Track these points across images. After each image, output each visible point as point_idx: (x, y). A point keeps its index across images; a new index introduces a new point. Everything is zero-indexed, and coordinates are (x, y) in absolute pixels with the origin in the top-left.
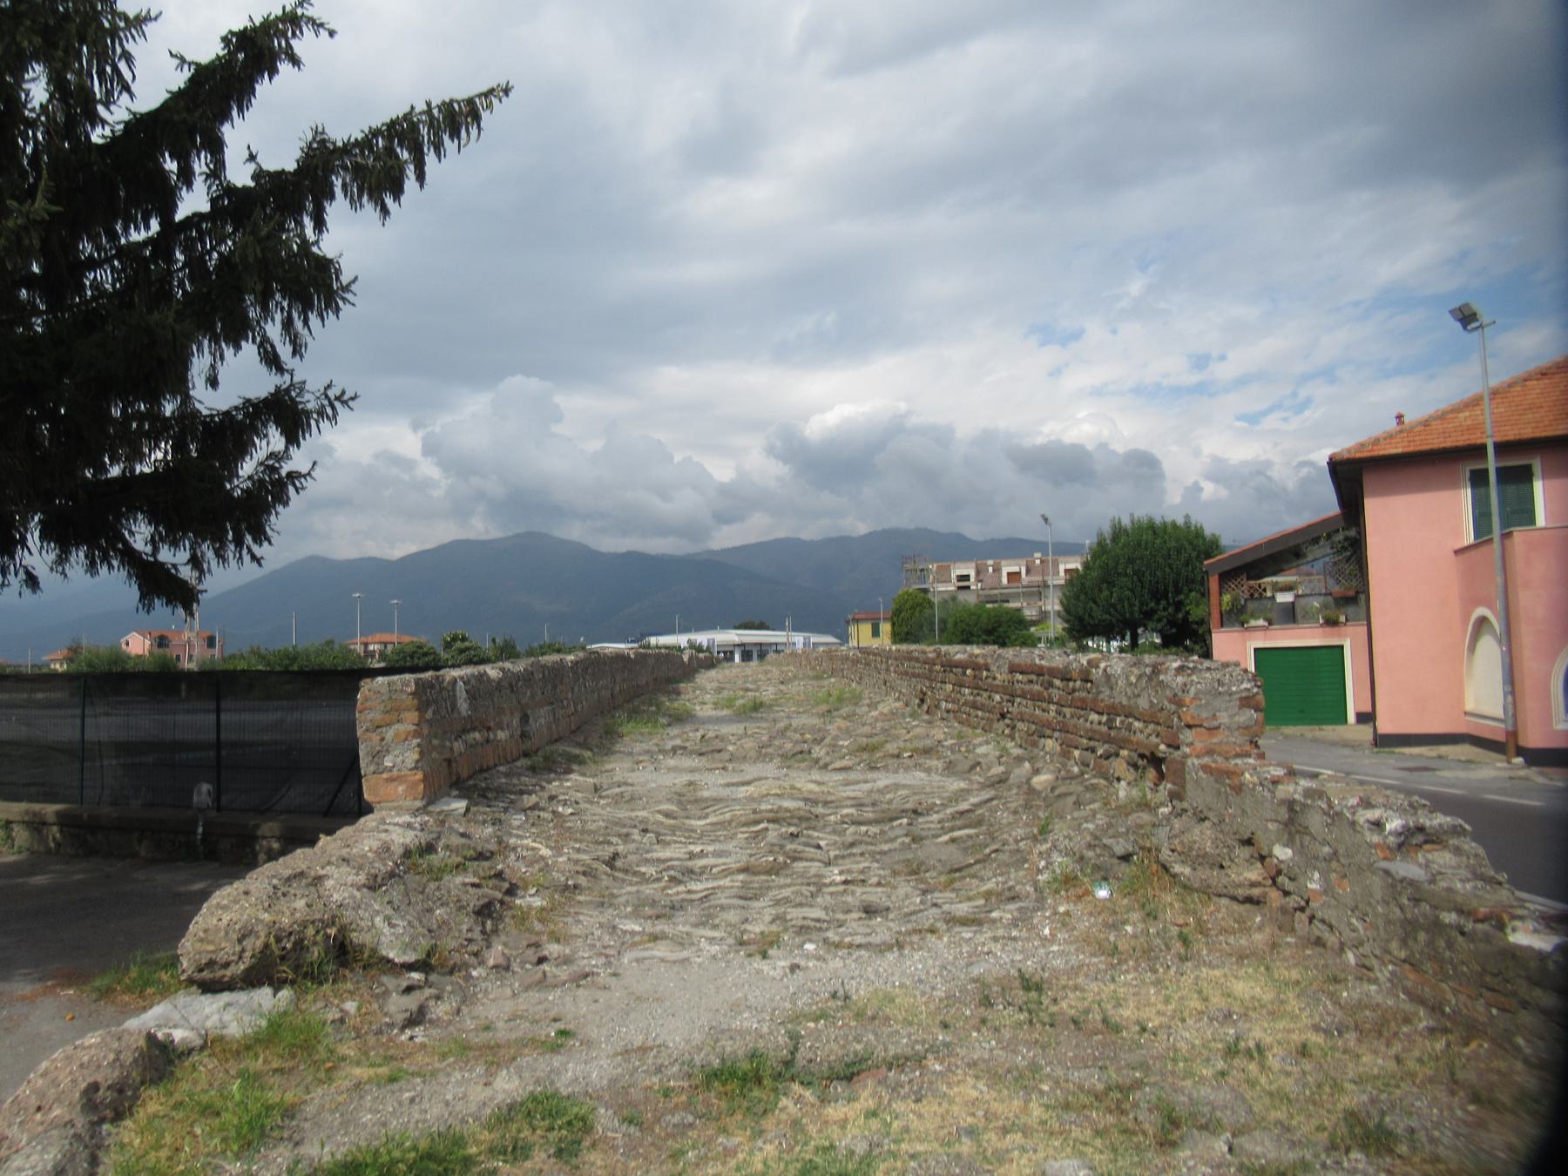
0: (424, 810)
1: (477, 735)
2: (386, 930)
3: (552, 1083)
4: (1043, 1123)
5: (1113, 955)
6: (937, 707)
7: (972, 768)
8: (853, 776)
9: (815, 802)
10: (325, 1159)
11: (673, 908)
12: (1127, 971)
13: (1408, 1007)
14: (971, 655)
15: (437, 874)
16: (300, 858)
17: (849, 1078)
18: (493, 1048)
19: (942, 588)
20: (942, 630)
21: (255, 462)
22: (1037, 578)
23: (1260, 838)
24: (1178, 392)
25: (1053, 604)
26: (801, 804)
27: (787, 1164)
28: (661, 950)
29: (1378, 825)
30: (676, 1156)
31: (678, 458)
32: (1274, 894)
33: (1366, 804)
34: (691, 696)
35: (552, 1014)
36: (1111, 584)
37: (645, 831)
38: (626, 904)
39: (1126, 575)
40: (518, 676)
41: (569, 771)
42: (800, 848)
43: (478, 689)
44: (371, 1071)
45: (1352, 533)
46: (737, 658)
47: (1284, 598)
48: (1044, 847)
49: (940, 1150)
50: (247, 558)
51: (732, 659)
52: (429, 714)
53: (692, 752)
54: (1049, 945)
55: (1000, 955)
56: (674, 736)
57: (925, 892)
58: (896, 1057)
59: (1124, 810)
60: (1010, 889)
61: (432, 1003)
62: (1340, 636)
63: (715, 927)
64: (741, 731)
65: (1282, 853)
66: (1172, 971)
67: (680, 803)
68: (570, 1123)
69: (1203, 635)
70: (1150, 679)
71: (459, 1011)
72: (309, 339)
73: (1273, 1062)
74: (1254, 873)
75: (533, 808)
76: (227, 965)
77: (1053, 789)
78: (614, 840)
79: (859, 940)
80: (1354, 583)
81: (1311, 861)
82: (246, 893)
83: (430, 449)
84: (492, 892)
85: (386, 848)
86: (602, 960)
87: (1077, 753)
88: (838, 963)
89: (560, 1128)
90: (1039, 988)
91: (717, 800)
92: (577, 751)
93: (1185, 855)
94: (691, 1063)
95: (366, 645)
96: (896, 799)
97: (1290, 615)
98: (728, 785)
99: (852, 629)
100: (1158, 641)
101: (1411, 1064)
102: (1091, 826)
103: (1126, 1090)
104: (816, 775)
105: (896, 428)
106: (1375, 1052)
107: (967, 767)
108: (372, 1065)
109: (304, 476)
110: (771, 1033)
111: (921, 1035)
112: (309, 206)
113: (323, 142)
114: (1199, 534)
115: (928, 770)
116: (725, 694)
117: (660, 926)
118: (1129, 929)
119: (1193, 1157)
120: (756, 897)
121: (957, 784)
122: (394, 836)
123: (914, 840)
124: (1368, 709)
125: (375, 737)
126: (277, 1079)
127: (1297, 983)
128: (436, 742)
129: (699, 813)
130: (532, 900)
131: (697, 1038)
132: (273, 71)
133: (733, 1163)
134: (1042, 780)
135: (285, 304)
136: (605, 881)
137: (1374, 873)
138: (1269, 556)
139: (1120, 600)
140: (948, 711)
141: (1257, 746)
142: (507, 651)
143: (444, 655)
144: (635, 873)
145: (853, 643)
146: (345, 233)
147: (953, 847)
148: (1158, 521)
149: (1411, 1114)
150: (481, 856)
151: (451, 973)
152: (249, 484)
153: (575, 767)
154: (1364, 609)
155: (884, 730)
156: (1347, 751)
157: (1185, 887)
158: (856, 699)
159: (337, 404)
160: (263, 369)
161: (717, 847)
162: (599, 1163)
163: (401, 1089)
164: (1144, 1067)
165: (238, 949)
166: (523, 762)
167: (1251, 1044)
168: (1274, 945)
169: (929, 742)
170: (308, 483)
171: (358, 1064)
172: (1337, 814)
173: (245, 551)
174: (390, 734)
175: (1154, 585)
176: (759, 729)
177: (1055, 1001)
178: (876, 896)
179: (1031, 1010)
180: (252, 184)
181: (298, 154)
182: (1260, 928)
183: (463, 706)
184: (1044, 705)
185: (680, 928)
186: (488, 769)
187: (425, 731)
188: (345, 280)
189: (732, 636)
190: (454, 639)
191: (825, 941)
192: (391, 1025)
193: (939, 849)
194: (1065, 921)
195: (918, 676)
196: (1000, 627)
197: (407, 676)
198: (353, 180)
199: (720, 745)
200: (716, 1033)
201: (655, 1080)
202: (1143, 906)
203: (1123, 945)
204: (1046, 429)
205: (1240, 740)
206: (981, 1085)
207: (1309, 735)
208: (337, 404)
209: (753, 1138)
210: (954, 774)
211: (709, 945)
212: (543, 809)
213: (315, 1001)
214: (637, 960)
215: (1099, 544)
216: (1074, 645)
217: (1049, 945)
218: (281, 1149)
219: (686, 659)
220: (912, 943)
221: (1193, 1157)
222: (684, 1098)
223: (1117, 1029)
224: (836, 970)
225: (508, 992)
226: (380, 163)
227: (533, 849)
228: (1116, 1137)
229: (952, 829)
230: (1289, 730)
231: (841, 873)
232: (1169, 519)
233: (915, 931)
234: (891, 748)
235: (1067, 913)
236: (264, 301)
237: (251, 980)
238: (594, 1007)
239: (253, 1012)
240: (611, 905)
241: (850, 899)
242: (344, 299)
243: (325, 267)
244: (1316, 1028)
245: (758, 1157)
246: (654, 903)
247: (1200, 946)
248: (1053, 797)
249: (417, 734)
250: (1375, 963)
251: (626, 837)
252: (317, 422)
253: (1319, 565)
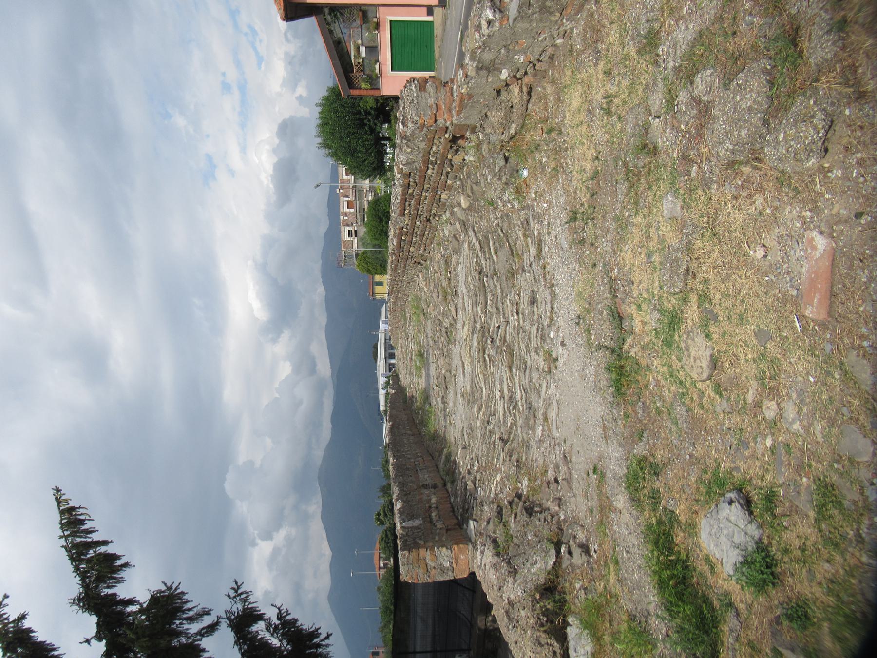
0: (474, 544)
1: (433, 514)
2: (538, 566)
3: (621, 478)
4: (644, 216)
5: (558, 172)
6: (422, 255)
7: (457, 239)
8: (460, 305)
9: (474, 328)
10: (656, 599)
11: (530, 408)
12: (567, 163)
13: (585, 14)
14: (394, 236)
15: (509, 537)
16: (498, 612)
17: (621, 318)
18: (602, 508)
19: (355, 246)
20: (380, 246)
21: (273, 639)
22: (351, 191)
23: (497, 85)
24: (244, 102)
25: (366, 184)
26: (475, 336)
27: (664, 354)
28: (552, 416)
29: (490, 22)
30: (659, 412)
31: (277, 395)
32: (526, 80)
33: (478, 28)
34: (414, 390)
35: (585, 476)
36: (355, 151)
37: (488, 422)
38: (527, 433)
39: (350, 142)
40: (401, 491)
41: (455, 461)
42: (499, 337)
43: (407, 514)
44: (612, 574)
45: (327, 10)
46: (393, 361)
47: (363, 52)
48: (500, 203)
49: (658, 273)
50: (327, 642)
51: (394, 365)
52: (421, 542)
53: (446, 393)
54: (553, 204)
55: (557, 232)
56: (437, 401)
57: (524, 271)
58: (611, 293)
59: (481, 158)
60: (522, 224)
61: (577, 540)
62: (385, 22)
63: (540, 385)
64: (434, 365)
65: (504, 74)
66: (567, 140)
67: (473, 402)
68: (641, 469)
69: (384, 100)
70: (409, 141)
71: (582, 526)
72: (200, 607)
73: (614, 90)
74: (515, 90)
75: (475, 484)
76: (554, 652)
77: (469, 197)
78: (493, 439)
79: (548, 308)
80: (355, 12)
81: (508, 60)
82: (516, 643)
83: (267, 536)
84: (519, 507)
85: (494, 566)
86: (557, 447)
87: (449, 182)
88: (561, 320)
89: (644, 473)
90: (575, 213)
91: (472, 382)
92: (444, 457)
93: (505, 127)
94: (612, 403)
95: (380, 568)
96: (473, 283)
97: (373, 49)
98: (464, 375)
99: (378, 297)
100: (387, 125)
101: (614, 16)
102: (489, 178)
103: (628, 171)
104: (459, 326)
105: (262, 268)
106: (608, 34)
107: (456, 242)
108: (609, 574)
109: (280, 611)
110: (597, 360)
111: (599, 279)
112: (120, 608)
113: (79, 599)
114: (327, 99)
115: (458, 264)
116: (413, 371)
117: (540, 415)
118: (544, 160)
119: (661, 137)
120: (525, 363)
121: (465, 249)
122: (488, 561)
123: (496, 275)
124: (425, 9)
125: (433, 572)
126: (615, 624)
127: (572, 71)
128: (437, 538)
129: (479, 392)
130: (524, 485)
131: (598, 399)
132: (30, 630)
133: (663, 382)
134: (464, 203)
135: (178, 622)
136: (515, 444)
137: (515, 27)
138: (340, 60)
139: (364, 146)
141: (447, 83)
142: (386, 490)
143: (388, 525)
144: (511, 428)
145: (386, 297)
146: (136, 587)
147: (499, 253)
148: (319, 122)
149: (639, 20)
150: (500, 513)
151: (562, 530)
152: (284, 641)
153: (452, 458)
154: (370, 8)
155: (435, 285)
156: (448, 23)
157: (522, 127)
158: (418, 299)
159: (239, 592)
160: (216, 633)
161: (497, 382)
162: (662, 453)
163: (622, 558)
164: (616, 159)
165: (546, 646)
166: (449, 486)
167: (604, 101)
168: (553, 82)
169: (442, 262)
170: (284, 609)
171: (608, 580)
172: (484, 44)
173: (323, 643)
174: (431, 564)
175: (356, 126)
176: (433, 354)
177: (582, 205)
178: (525, 297)
179: (587, 218)
180: (104, 641)
181: (86, 614)
182: (544, 89)
183: (417, 522)
184: (423, 198)
185: (541, 405)
186: (453, 508)
187: (431, 544)
188: (163, 588)
189: (381, 364)
190: (378, 519)
191: (549, 326)
192: (588, 562)
193: (501, 261)
194: (540, 195)
195: (405, 265)
196: (378, 215)
197: (399, 555)
198: (105, 582)
199: (442, 377)
200: (596, 389)
201: (620, 422)
202: (532, 152)
203: (553, 165)
204: (265, 182)
206: (625, 249)
207: (439, 43)
208: (239, 592)
209: (651, 371)
210: (460, 249)
211: (550, 389)
212: (475, 478)
213: (575, 604)
214: (557, 429)
215: (332, 156)
216: (388, 173)
217: (553, 204)
218: (652, 622)
219: (393, 392)
220: (550, 279)
221: (661, 137)
222: (629, 407)
223: (597, 172)
224: (565, 321)
225: (573, 499)
226: (95, 567)
227: (497, 484)
228: (652, 178)
229: (490, 253)
230: (437, 54)
231: (513, 315)
232: (318, 116)
233: (544, 277)
234: (445, 283)
235: (536, 193)
236: (178, 634)
237: (563, 639)
238: (582, 453)
239: (580, 638)
240: (528, 442)
241: (527, 312)
242: (176, 589)
243: (155, 599)
244: (596, 65)
245: (660, 368)
246: (527, 419)
247: (554, 122)
248: (472, 196)
249: (432, 549)
250: (562, 29)
251: (491, 433)
252: (250, 603)
253: (345, 31)
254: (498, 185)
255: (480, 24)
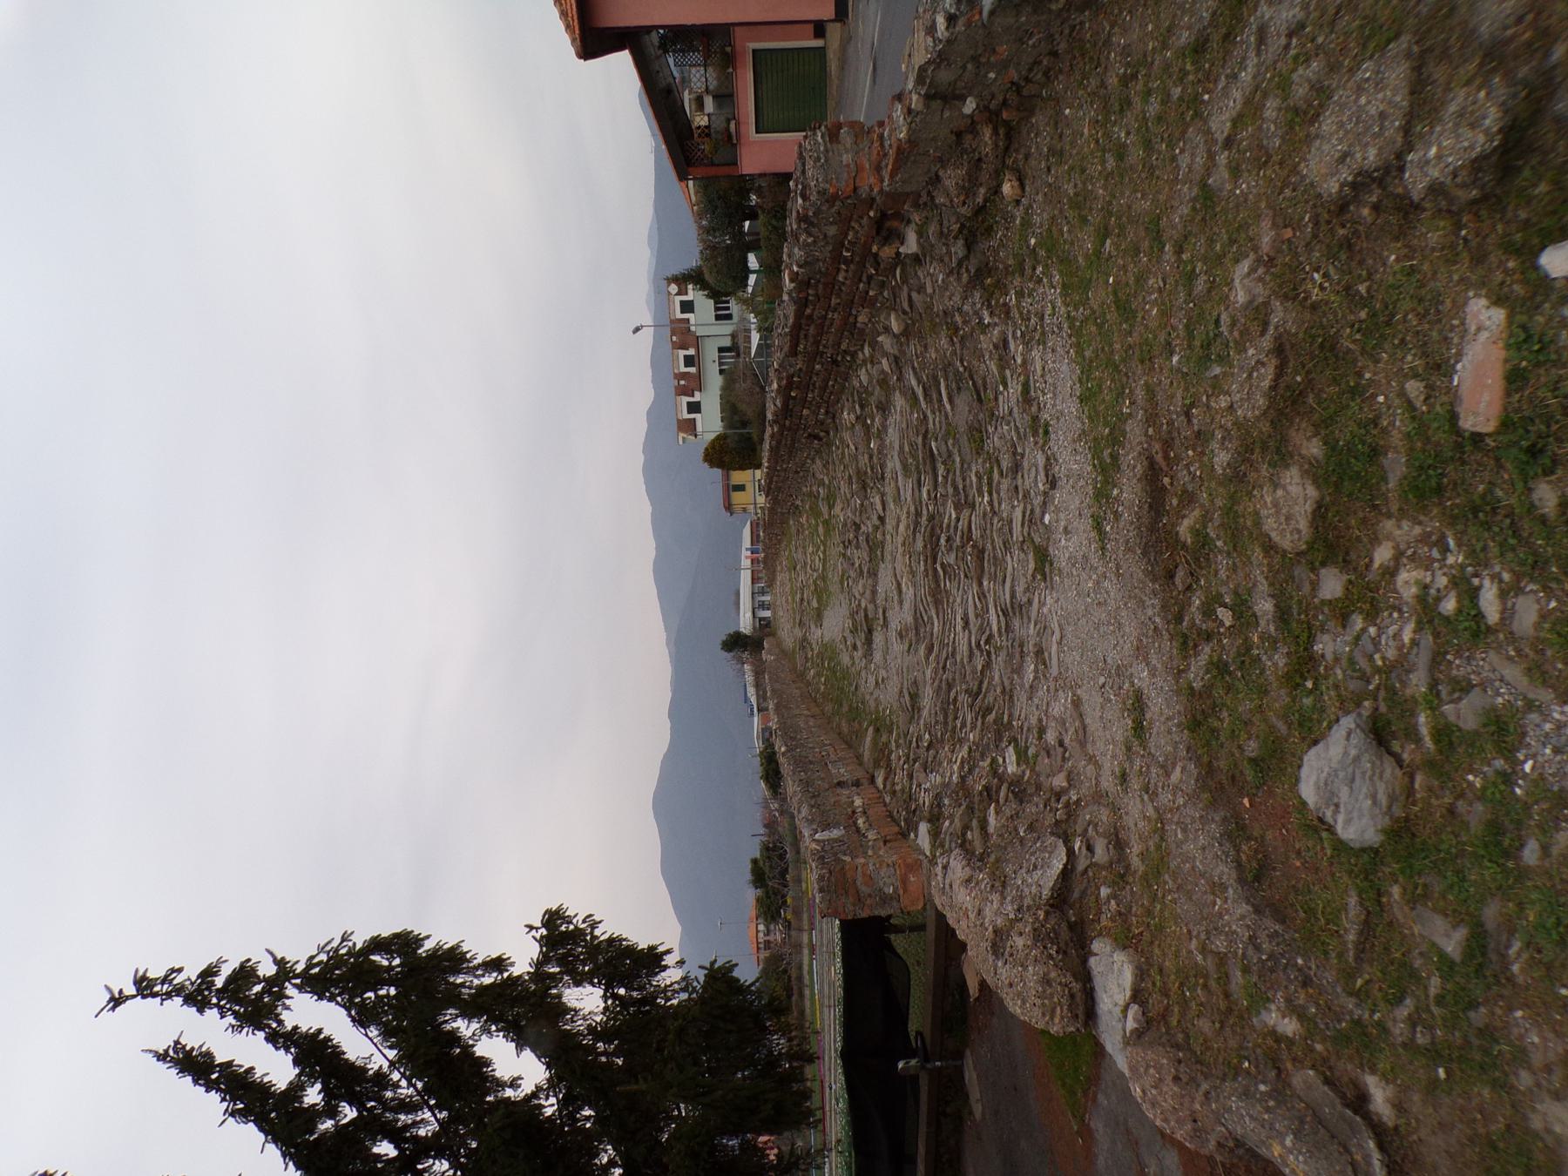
1: (860, 821)
9: (917, 523)
14: (778, 391)
63: (1030, 602)
65: (970, 106)
78: (952, 695)
121: (899, 401)
124: (811, 28)
140: (827, 412)
147: (957, 401)
183: (836, 833)
193: (962, 411)
205: (866, 143)
210: (888, 401)
229: (940, 400)
231: (981, 494)
254: (957, 289)
255: (934, 22)
